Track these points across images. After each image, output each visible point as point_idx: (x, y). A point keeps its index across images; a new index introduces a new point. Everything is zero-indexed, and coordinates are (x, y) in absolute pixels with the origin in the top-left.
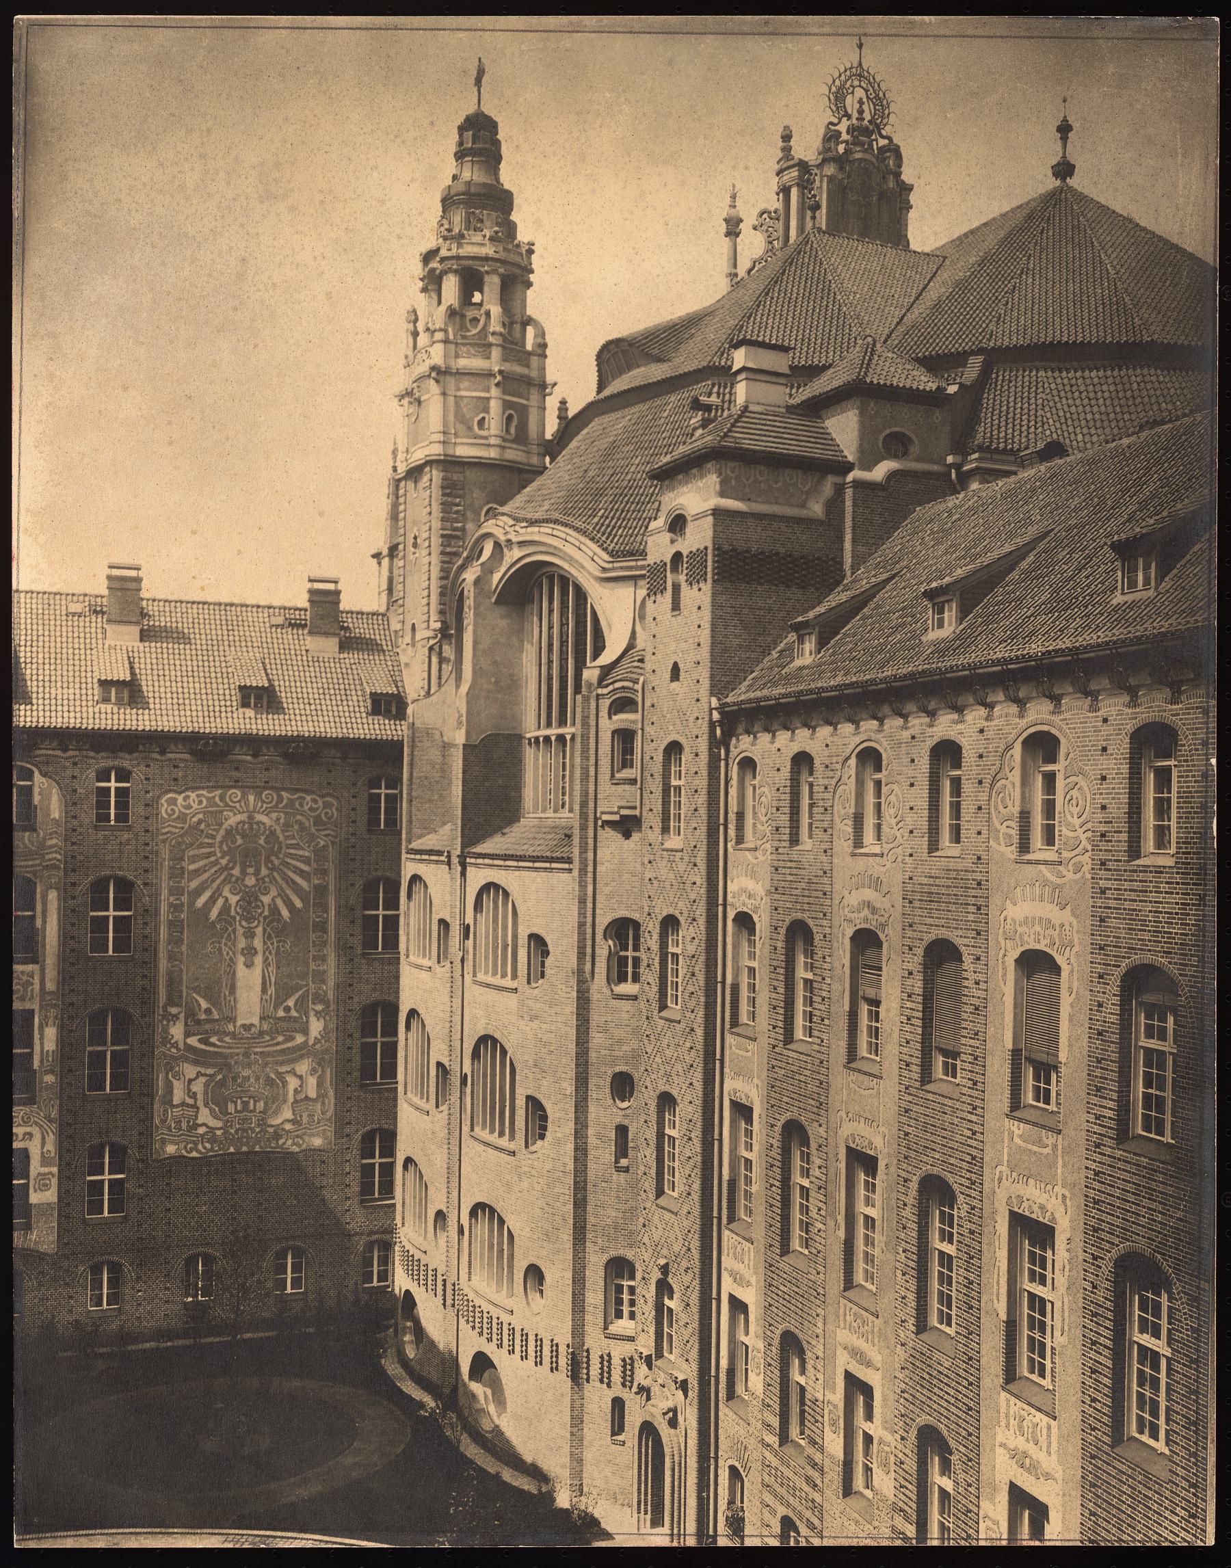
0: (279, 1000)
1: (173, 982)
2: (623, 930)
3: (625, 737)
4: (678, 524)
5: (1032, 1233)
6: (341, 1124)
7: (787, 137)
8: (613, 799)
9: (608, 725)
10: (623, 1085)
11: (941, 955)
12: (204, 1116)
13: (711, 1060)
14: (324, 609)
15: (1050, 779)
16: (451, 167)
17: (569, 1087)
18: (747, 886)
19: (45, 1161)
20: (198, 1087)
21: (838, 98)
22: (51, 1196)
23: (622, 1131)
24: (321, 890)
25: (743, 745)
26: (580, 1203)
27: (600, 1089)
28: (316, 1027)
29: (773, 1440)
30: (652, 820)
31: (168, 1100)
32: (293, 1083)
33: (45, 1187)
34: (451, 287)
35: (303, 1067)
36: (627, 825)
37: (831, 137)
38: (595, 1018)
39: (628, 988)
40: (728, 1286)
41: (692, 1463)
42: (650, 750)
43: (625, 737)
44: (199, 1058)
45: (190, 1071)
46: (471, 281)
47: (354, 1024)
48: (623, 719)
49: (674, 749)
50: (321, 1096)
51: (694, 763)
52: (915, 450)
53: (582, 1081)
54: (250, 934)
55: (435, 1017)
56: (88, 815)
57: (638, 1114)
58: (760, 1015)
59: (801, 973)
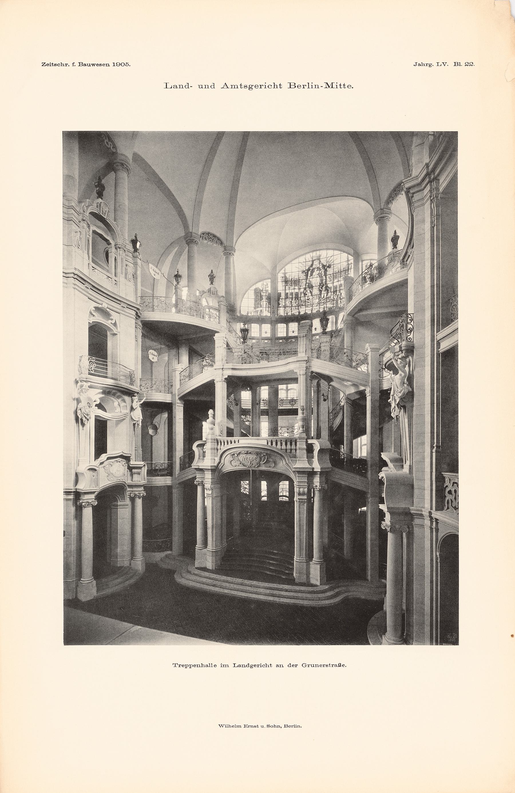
40: (322, 392)
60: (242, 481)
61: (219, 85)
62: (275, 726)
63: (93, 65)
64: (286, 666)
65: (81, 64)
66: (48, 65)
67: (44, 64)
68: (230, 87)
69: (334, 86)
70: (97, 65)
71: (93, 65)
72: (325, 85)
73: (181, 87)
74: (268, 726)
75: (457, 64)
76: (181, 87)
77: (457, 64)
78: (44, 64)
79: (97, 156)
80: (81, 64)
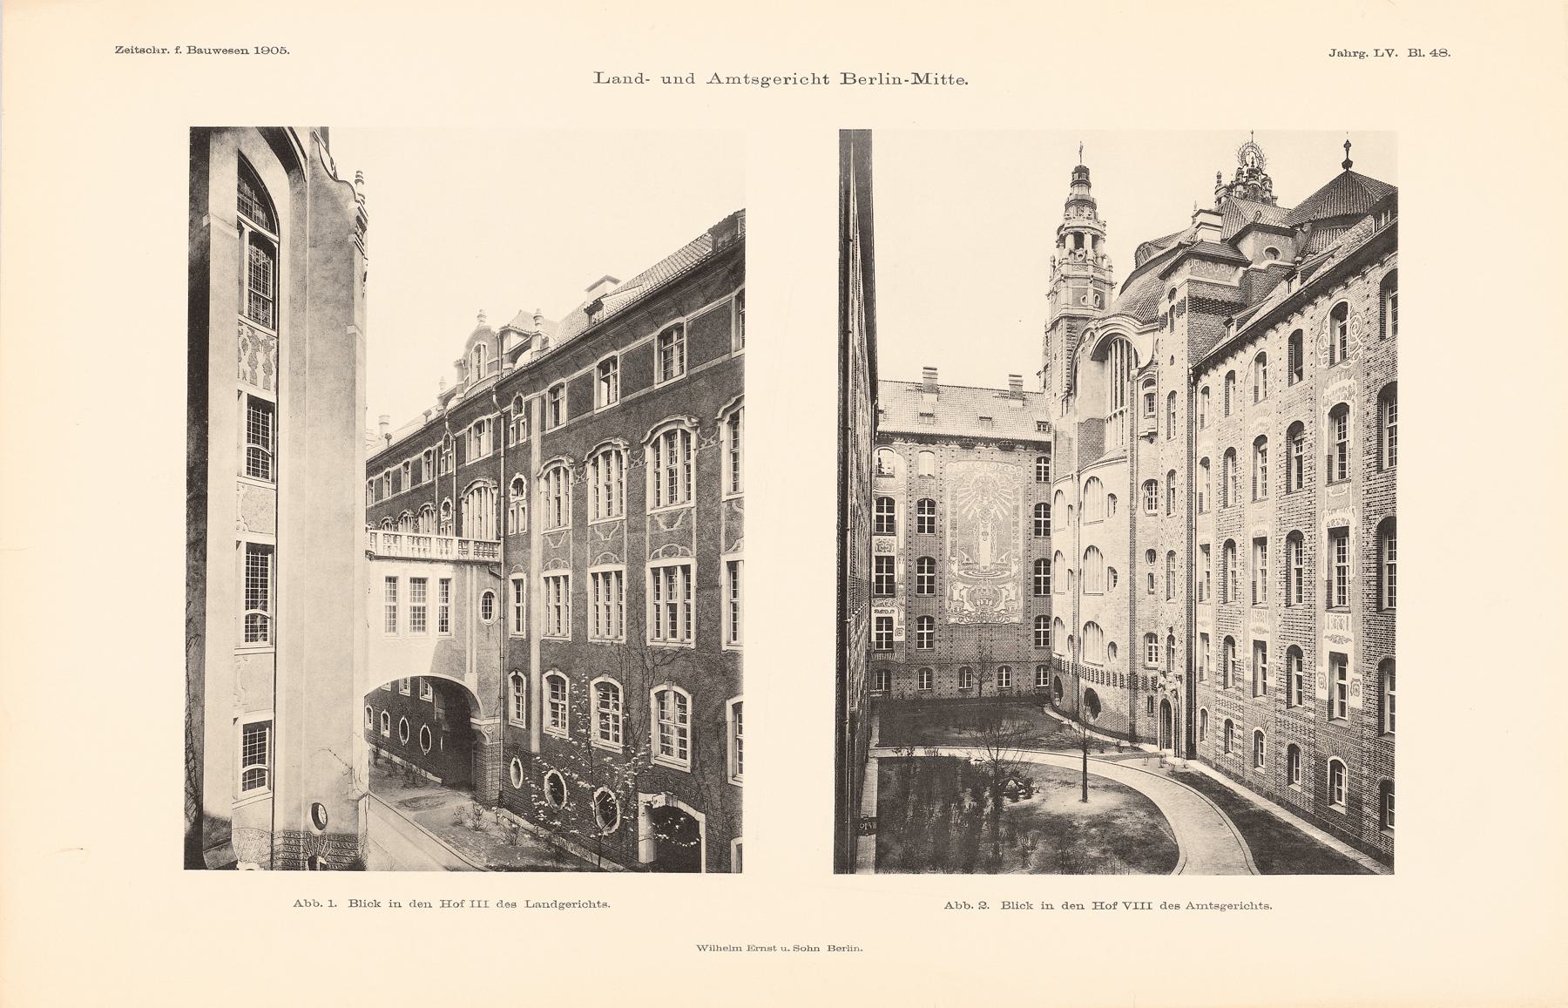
0: (1000, 553)
1: (953, 546)
2: (1150, 483)
3: (1150, 396)
4: (1173, 292)
5: (1339, 660)
6: (1027, 610)
7: (1219, 177)
8: (1145, 426)
9: (1142, 393)
10: (1152, 554)
11: (1295, 538)
12: (967, 606)
13: (1191, 529)
14: (1016, 392)
15: (1343, 330)
16: (1070, 190)
17: (1127, 559)
18: (1207, 533)
19: (900, 623)
20: (964, 593)
21: (1243, 156)
22: (902, 638)
23: (1151, 576)
24: (1017, 508)
25: (1205, 381)
26: (1133, 611)
27: (1141, 556)
28: (1015, 569)
29: (1220, 688)
30: (1163, 432)
31: (951, 599)
32: (1005, 593)
33: (899, 634)
34: (1070, 241)
35: (1009, 586)
36: (1151, 437)
37: (1240, 173)
38: (1138, 526)
39: (1154, 511)
40: (1200, 629)
41: (1184, 712)
42: (1161, 401)
43: (1150, 396)
44: (963, 580)
45: (960, 585)
46: (1079, 238)
47: (1031, 568)
48: (1149, 390)
49: (1173, 394)
50: (1017, 599)
51: (1182, 398)
52: (1280, 257)
53: (1132, 554)
54: (985, 526)
55: (1067, 619)
56: (914, 644)
57: (1159, 568)
58: (1212, 500)
59: (1230, 474)
60: (566, 642)
61: (703, 76)
62: (590, 904)
63: (217, 51)
64: (1058, 906)
65: (193, 50)
66: (127, 51)
67: (119, 50)
68: (724, 80)
69: (931, 80)
70: (225, 51)
71: (217, 51)
72: (912, 78)
73: (628, 80)
74: (796, 948)
75: (1415, 53)
76: (628, 80)
77: (1415, 53)
78: (119, 50)
79: (1342, 236)
80: (193, 50)
